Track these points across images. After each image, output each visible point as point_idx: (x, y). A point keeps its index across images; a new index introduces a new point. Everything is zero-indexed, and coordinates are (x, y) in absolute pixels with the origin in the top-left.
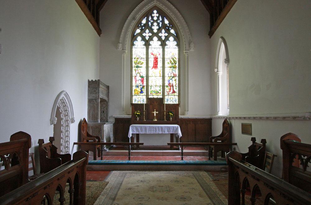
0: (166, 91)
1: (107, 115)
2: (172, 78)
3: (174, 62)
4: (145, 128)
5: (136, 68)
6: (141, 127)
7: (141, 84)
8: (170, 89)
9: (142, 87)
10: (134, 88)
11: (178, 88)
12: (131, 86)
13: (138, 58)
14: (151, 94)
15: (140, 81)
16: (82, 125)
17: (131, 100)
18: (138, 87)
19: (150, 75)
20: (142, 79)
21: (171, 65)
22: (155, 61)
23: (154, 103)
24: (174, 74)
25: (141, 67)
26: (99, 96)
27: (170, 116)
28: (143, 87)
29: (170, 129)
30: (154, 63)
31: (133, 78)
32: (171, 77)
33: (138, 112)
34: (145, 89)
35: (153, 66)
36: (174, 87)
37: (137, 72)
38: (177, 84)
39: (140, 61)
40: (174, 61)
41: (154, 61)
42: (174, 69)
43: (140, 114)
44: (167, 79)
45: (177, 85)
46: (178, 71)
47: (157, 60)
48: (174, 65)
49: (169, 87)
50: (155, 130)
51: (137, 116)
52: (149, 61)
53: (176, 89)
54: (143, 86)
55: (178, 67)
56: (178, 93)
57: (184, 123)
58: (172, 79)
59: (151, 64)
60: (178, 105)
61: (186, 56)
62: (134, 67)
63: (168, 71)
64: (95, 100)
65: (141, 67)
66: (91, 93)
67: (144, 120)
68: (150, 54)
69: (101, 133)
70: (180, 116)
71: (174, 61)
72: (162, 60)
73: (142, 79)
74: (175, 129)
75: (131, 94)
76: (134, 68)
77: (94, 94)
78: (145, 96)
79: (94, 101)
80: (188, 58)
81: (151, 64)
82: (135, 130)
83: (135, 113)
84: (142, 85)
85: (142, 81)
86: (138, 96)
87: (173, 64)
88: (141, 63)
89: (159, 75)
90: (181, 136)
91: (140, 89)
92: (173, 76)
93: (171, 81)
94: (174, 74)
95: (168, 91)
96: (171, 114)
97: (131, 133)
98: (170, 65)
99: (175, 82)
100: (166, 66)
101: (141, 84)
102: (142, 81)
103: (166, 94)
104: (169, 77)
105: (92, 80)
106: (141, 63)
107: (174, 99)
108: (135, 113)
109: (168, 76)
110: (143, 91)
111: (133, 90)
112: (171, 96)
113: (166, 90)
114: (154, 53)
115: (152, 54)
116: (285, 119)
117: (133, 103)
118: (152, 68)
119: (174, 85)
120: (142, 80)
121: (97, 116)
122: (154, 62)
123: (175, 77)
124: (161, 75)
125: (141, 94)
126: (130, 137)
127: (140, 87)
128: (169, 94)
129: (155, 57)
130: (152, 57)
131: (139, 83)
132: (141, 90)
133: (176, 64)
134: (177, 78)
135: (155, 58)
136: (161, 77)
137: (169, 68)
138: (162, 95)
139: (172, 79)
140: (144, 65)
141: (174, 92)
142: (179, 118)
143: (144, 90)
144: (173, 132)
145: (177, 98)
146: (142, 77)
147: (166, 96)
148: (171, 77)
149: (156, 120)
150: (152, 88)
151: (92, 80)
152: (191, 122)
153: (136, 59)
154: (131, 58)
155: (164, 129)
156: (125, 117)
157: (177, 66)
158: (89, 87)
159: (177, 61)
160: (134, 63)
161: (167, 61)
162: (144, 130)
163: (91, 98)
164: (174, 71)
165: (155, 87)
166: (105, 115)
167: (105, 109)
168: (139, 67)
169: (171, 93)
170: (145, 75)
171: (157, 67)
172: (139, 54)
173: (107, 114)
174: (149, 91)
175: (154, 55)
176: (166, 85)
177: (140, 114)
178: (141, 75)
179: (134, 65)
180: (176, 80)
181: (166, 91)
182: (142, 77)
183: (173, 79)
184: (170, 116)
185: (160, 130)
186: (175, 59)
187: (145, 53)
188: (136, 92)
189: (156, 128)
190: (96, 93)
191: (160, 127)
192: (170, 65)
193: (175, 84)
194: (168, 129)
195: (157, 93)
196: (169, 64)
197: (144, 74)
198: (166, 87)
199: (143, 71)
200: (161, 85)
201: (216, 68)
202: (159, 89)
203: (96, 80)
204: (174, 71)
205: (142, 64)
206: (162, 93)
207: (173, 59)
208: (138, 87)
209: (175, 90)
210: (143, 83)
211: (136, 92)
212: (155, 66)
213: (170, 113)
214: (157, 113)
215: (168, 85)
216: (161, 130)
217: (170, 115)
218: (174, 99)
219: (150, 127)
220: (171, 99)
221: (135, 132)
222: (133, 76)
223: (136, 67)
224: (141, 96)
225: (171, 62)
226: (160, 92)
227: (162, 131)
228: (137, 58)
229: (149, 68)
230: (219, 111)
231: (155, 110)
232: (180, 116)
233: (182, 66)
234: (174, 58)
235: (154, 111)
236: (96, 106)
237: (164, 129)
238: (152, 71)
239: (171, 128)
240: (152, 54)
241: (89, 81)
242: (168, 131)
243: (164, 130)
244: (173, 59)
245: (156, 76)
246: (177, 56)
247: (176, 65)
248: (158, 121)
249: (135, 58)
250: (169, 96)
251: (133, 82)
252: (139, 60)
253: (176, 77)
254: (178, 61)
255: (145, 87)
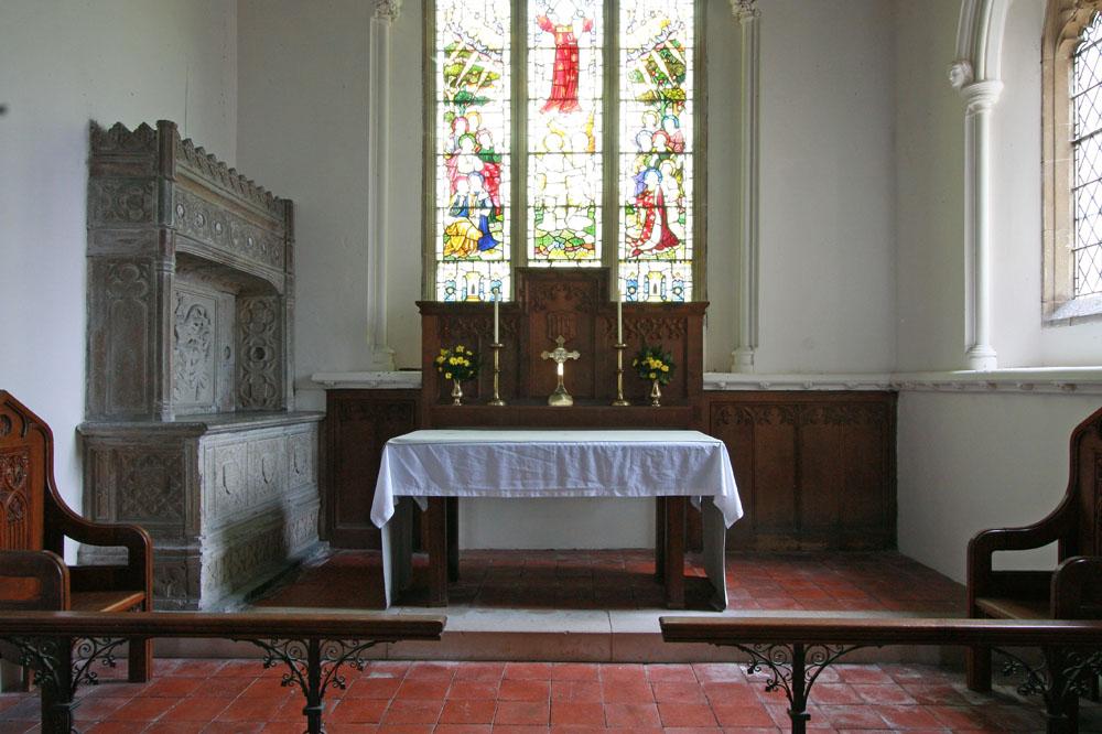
0: (627, 236)
1: (280, 372)
2: (661, 160)
3: (673, 72)
4: (484, 457)
5: (457, 109)
6: (460, 453)
7: (486, 195)
8: (648, 225)
9: (486, 212)
10: (444, 219)
11: (694, 214)
12: (428, 210)
13: (465, 50)
14: (538, 250)
15: (476, 182)
16: (84, 440)
17: (423, 285)
18: (463, 211)
19: (534, 142)
20: (487, 169)
21: (654, 87)
22: (560, 68)
23: (554, 298)
24: (669, 140)
25: (484, 101)
26: (163, 234)
27: (653, 376)
28: (497, 211)
29: (657, 465)
30: (555, 77)
31: (440, 161)
32: (651, 153)
33: (457, 355)
34: (507, 224)
35: (548, 94)
36: (672, 214)
37: (461, 126)
38: (689, 197)
39: (480, 64)
40: (670, 62)
41: (555, 65)
42: (669, 112)
43: (467, 363)
44: (628, 165)
45: (688, 203)
46: (691, 118)
47: (574, 58)
48: (669, 86)
49: (643, 212)
50: (554, 471)
51: (448, 376)
52: (531, 68)
53: (682, 222)
54: (494, 207)
55: (695, 100)
56: (690, 244)
57: (726, 414)
58: (656, 168)
59: (540, 84)
60: (698, 308)
61: (746, 21)
62: (447, 101)
63: (635, 120)
64: (140, 262)
65: (484, 101)
66: (108, 217)
67: (494, 400)
68: (533, 28)
69: (181, 493)
70: (711, 378)
71: (670, 62)
72: (600, 61)
73: (491, 167)
74: (694, 465)
75: (424, 257)
76: (442, 109)
77: (127, 218)
78: (507, 265)
79: (131, 274)
80: (755, 28)
81: (540, 84)
82: (418, 475)
83: (441, 359)
84: (489, 204)
85: (491, 180)
86: (467, 266)
87: (662, 81)
88: (484, 76)
89: (581, 144)
90: (740, 513)
91: (477, 222)
92: (663, 149)
93: (651, 179)
94: (669, 140)
95: (635, 233)
96: (656, 364)
97: (389, 490)
98: (650, 86)
99: (673, 182)
100: (622, 95)
101: (481, 197)
102: (491, 180)
103: (622, 255)
104: (642, 158)
105: (119, 126)
106: (484, 76)
107: (669, 281)
108: (441, 359)
109: (636, 149)
110: (496, 237)
111: (440, 231)
112: (656, 266)
113: (622, 229)
114: (555, 23)
115: (547, 27)
116: (1076, 391)
117: (441, 298)
118: (544, 103)
119: (670, 202)
120: (487, 174)
121: (150, 375)
122: (555, 71)
123: (677, 154)
124: (599, 148)
125: (485, 255)
126: (380, 525)
127: (478, 213)
128: (641, 252)
129: (560, 40)
130: (548, 40)
131: (473, 188)
132: (480, 229)
133: (681, 79)
134: (688, 162)
135: (559, 49)
136: (599, 158)
137: (642, 107)
138: (599, 256)
139: (656, 168)
140: (501, 92)
141: (669, 240)
142: (705, 388)
143: (502, 231)
144: (678, 482)
145: (685, 271)
146: (490, 158)
147: (622, 265)
148: (651, 153)
149: (565, 401)
150: (548, 218)
151: (119, 126)
152: (775, 412)
153: (454, 54)
154: (428, 51)
155: (622, 467)
156: (381, 382)
157: (690, 95)
158: (95, 172)
159: (690, 66)
160: (447, 77)
161: (633, 66)
162: (478, 469)
163: (105, 250)
164: (669, 125)
165: (561, 212)
166: (269, 372)
167: (268, 334)
168: (472, 102)
169: (649, 244)
170: (508, 144)
171: (574, 99)
172: (470, 25)
173: (279, 365)
174: (530, 234)
175: (555, 33)
176: (622, 203)
177: (467, 363)
178: (486, 147)
179: (442, 87)
180: (679, 172)
181: (622, 238)
182: (490, 158)
183: (667, 167)
184: (653, 376)
185: (593, 475)
186: (675, 53)
187: (507, 24)
188: (457, 242)
189: (561, 461)
190: (147, 217)
191: (591, 453)
192: (650, 86)
193: (677, 192)
194: (643, 466)
195: (576, 244)
196: (641, 79)
197: (499, 138)
198: (622, 212)
199: (493, 123)
200: (599, 202)
201: (959, 61)
202: (581, 223)
203: (144, 127)
204: (669, 125)
205: (488, 82)
206: (599, 246)
207: (664, 52)
208: (463, 211)
209: (675, 229)
210: (493, 192)
211: (457, 242)
212: (565, 92)
213: (651, 361)
214: (575, 355)
215: (633, 201)
216: (599, 468)
217: (648, 368)
218: (669, 281)
219: (521, 450)
220: (655, 280)
221: (421, 489)
222: (440, 151)
223: (455, 102)
224: (482, 267)
225: (652, 69)
226: (589, 240)
227: (604, 479)
228: (460, 47)
229: (531, 104)
230: (975, 345)
231: (561, 340)
232: (711, 378)
233: (713, 67)
234: (669, 45)
235: (553, 347)
236: (145, 305)
237: (616, 464)
238: (543, 125)
239: (666, 461)
240: (547, 27)
241: (95, 131)
242: (647, 479)
243: (615, 471)
244: (664, 52)
245: (565, 150)
246: (686, 38)
247: (682, 86)
248: (663, 408)
249: (448, 53)
250: (643, 265)
251: (439, 183)
252: (471, 61)
253: (681, 158)
254: (694, 61)
255: (507, 213)
